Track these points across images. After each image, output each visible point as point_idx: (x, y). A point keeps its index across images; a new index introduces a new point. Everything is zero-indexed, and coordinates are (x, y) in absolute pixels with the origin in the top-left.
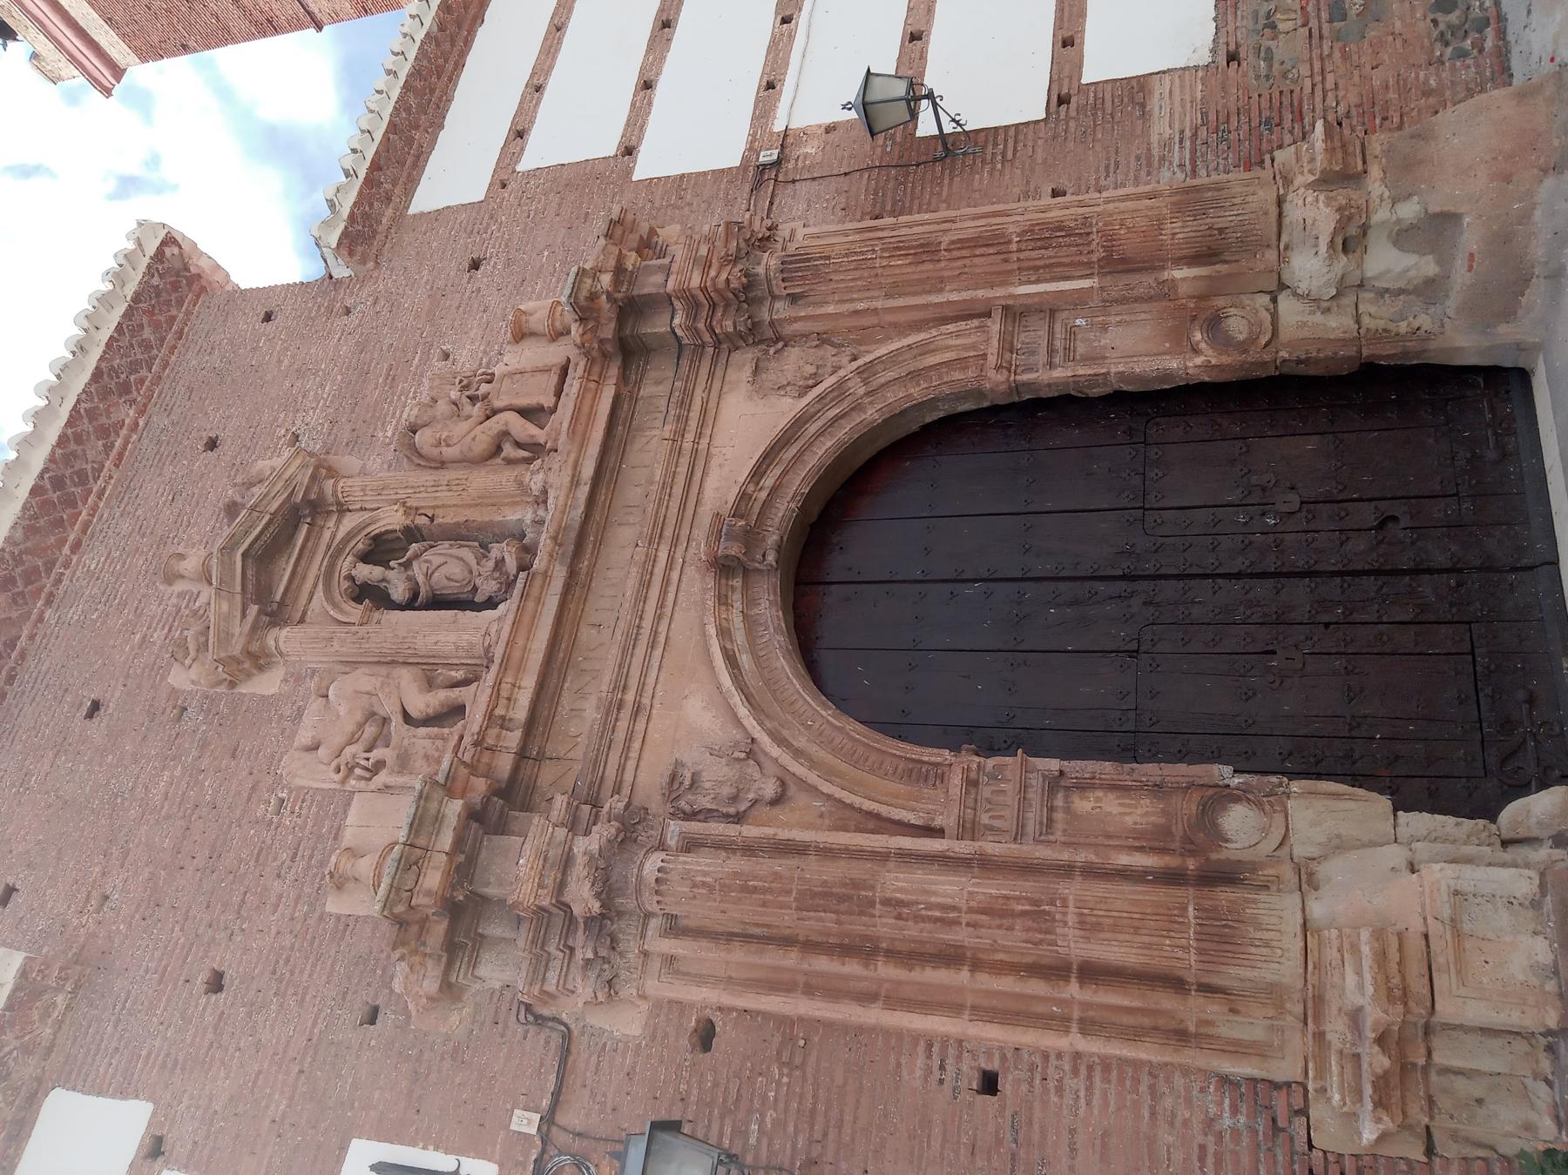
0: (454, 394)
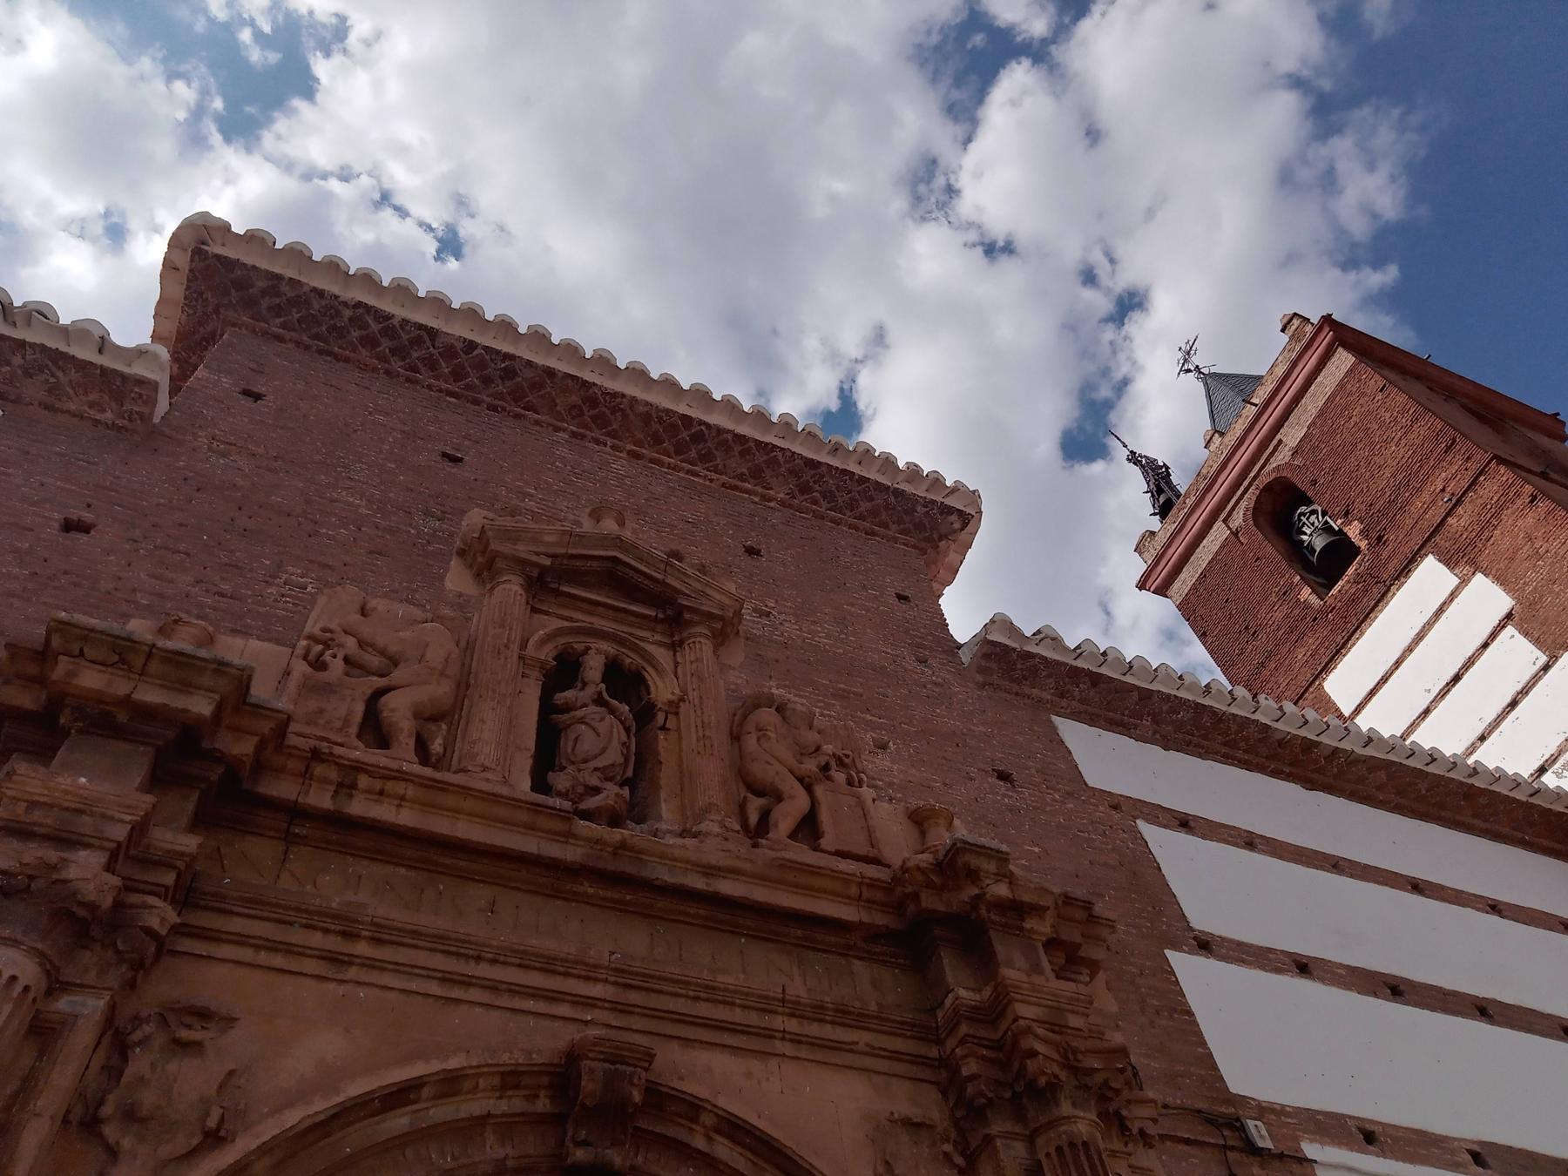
0: (828, 748)
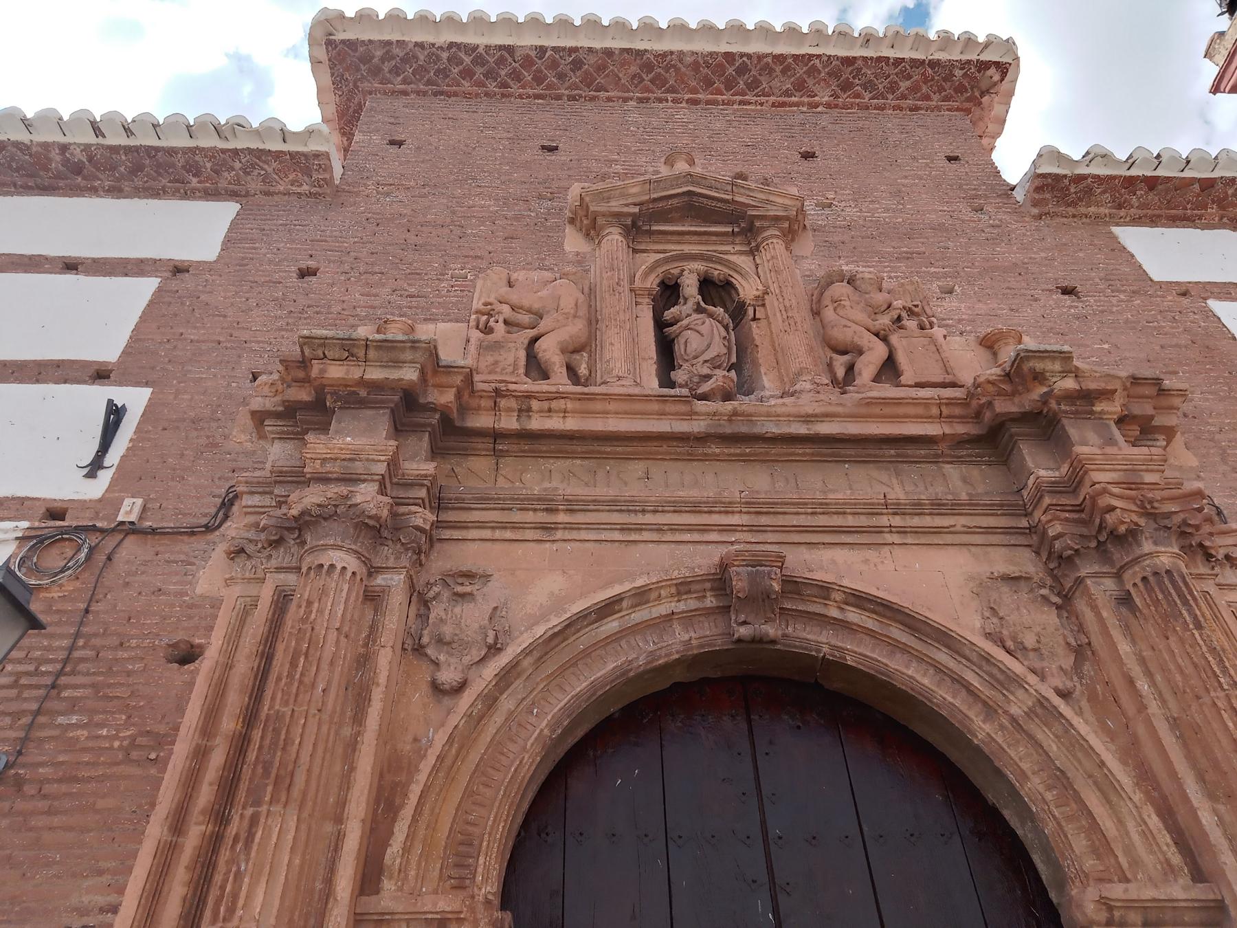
0: (898, 303)
